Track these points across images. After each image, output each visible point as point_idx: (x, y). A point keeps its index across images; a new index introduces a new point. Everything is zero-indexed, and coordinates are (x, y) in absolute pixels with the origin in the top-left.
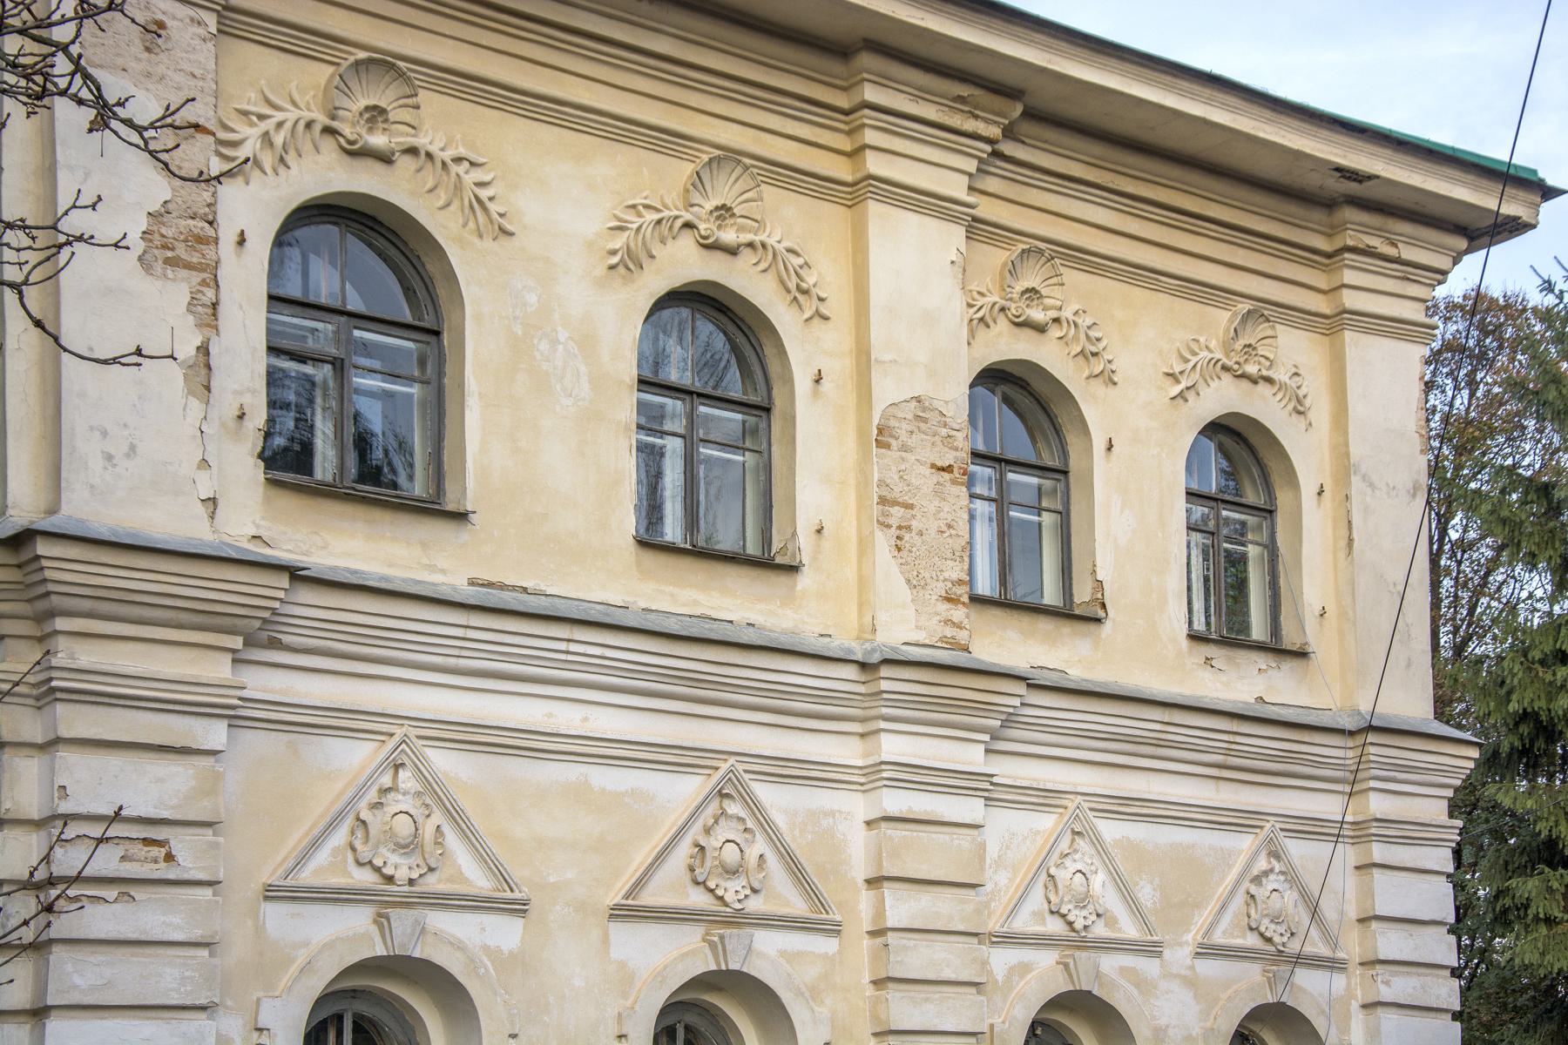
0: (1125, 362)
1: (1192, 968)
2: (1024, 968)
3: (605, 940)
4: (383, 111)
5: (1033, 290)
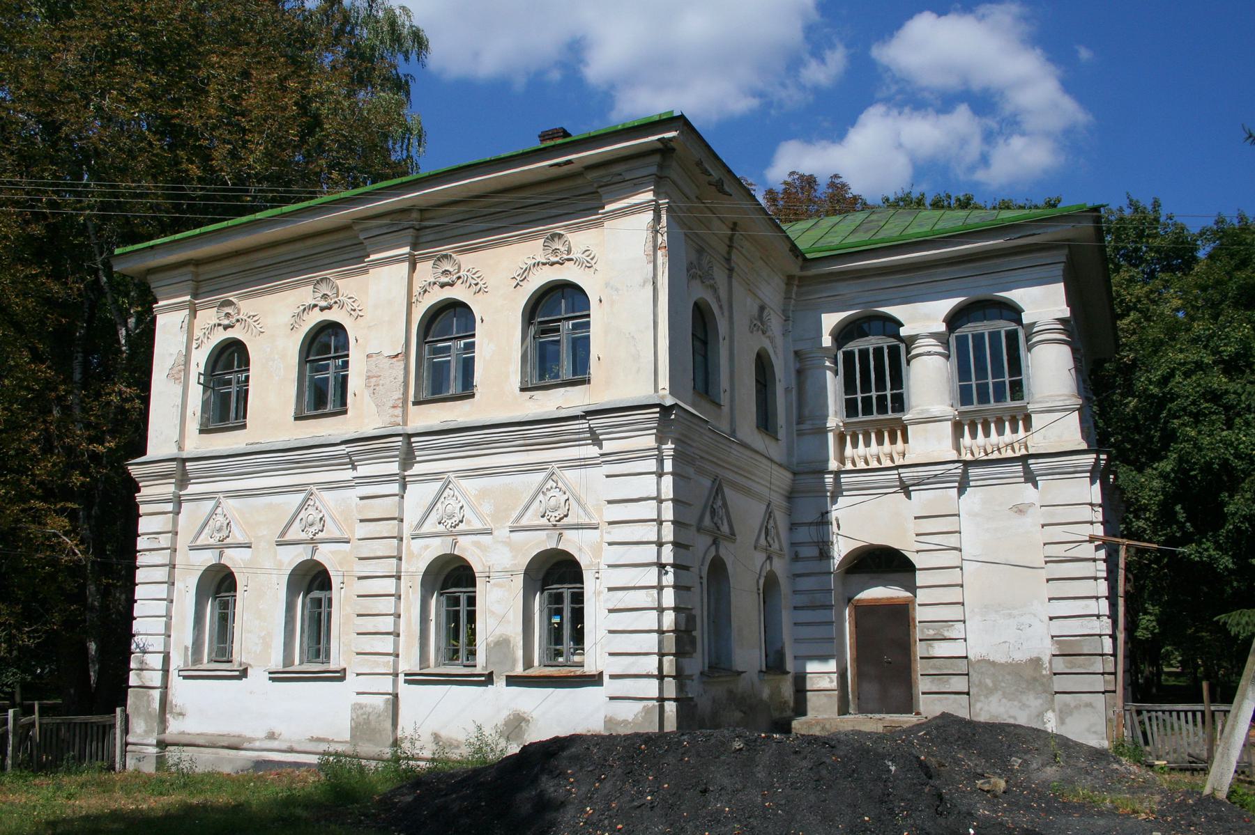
0: (491, 281)
1: (509, 537)
2: (427, 547)
3: (276, 552)
4: (229, 314)
5: (324, 294)
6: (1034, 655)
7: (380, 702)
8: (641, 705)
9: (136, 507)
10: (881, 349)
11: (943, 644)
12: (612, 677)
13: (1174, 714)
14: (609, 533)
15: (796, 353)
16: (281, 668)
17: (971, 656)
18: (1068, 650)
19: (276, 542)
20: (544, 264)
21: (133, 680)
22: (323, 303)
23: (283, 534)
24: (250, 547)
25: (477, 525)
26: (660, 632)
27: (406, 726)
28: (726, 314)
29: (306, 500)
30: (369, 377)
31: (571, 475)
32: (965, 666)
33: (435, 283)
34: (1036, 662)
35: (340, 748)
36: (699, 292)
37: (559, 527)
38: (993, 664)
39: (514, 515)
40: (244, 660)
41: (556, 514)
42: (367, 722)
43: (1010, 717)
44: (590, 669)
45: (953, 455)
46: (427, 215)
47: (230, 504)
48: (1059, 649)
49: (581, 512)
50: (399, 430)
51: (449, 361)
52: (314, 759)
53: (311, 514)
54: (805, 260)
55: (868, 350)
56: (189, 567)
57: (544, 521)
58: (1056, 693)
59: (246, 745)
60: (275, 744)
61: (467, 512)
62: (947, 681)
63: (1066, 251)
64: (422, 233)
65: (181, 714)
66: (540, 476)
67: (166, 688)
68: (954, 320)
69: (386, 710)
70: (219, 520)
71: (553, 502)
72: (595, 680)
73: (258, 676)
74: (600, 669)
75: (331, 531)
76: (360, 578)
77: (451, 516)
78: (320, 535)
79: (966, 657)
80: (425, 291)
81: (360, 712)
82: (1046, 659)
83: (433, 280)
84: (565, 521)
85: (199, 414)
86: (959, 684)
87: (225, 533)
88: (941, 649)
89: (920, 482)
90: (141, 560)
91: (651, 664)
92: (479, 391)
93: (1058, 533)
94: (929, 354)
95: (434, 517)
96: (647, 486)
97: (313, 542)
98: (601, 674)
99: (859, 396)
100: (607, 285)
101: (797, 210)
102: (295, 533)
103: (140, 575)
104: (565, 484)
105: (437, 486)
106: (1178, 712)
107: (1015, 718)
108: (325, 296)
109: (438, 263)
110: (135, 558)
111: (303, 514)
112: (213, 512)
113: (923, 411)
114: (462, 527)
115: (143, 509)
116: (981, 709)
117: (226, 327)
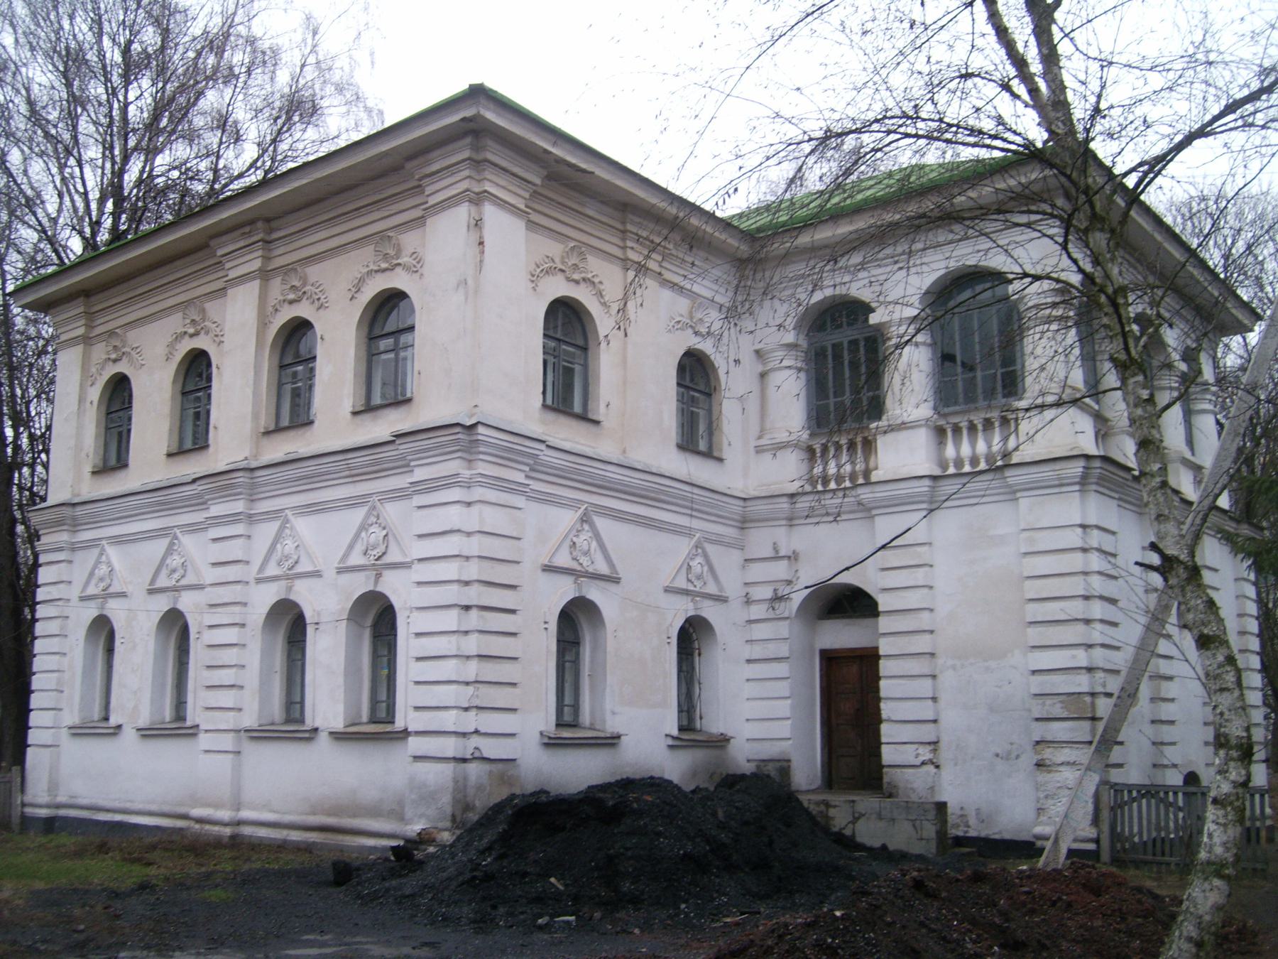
15: (757, 352)
19: (337, 568)
20: (377, 271)
22: (191, 331)
23: (153, 581)
29: (171, 544)
33: (284, 301)
36: (557, 288)
44: (399, 724)
46: (274, 224)
47: (113, 552)
53: (175, 561)
55: (841, 344)
64: (272, 246)
70: (103, 570)
72: (405, 734)
73: (129, 734)
78: (183, 582)
80: (276, 310)
83: (282, 298)
95: (359, 547)
101: (1183, 215)
102: (163, 582)
109: (287, 278)
112: (98, 563)
117: (115, 361)
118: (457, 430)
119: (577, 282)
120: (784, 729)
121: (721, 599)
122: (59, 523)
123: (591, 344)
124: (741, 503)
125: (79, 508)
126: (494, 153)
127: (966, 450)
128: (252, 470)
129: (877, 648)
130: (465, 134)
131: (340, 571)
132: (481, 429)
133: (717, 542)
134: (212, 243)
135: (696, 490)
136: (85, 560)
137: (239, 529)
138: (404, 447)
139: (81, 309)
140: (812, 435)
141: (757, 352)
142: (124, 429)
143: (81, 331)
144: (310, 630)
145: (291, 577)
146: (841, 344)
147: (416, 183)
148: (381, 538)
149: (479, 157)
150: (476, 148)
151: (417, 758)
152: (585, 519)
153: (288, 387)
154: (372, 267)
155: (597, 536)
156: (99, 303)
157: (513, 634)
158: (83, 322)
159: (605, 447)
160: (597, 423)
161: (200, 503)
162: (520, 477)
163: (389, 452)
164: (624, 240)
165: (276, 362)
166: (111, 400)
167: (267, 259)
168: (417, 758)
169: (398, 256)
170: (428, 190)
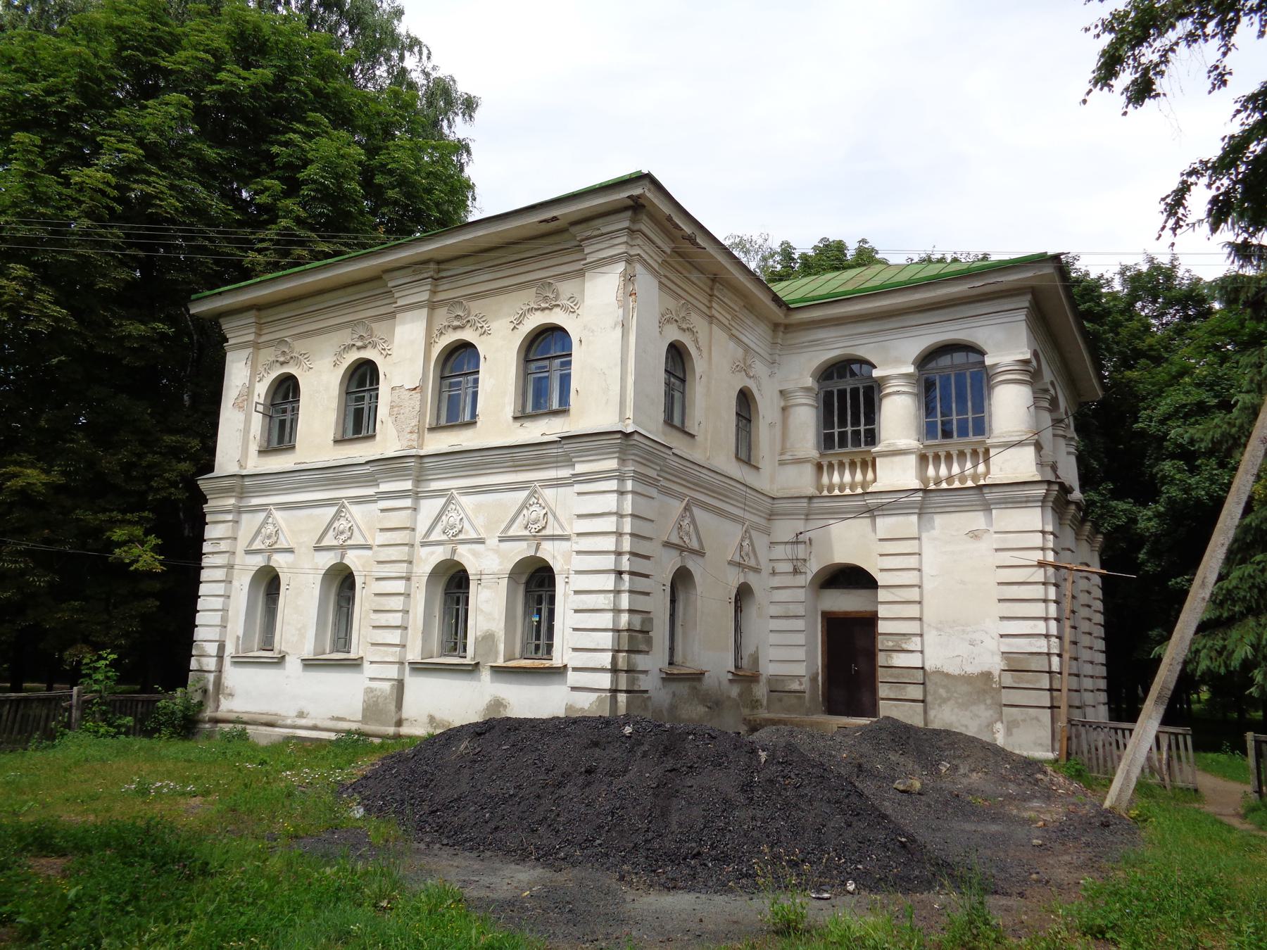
2: (433, 553)
6: (985, 669)
7: (387, 686)
8: (595, 695)
9: (204, 515)
10: (858, 389)
11: (902, 655)
12: (575, 669)
13: (1120, 732)
14: (577, 543)
15: (781, 392)
16: (312, 657)
17: (927, 667)
18: (1016, 665)
20: (536, 309)
21: (194, 664)
22: (359, 344)
24: (293, 552)
25: (473, 535)
26: (616, 630)
27: (409, 710)
28: (705, 354)
29: (339, 511)
30: (392, 407)
31: (549, 494)
32: (924, 676)
34: (987, 676)
35: (354, 726)
36: (673, 334)
37: (539, 537)
38: (947, 675)
39: (503, 527)
40: (283, 649)
41: (536, 526)
42: (376, 704)
43: (963, 726)
44: (557, 661)
45: (916, 484)
46: (442, 267)
47: (279, 515)
48: (1008, 665)
49: (556, 525)
50: (413, 452)
51: (459, 395)
52: (332, 736)
53: (342, 524)
54: (789, 309)
55: (845, 390)
56: (244, 569)
57: (526, 533)
58: (1005, 705)
59: (280, 722)
60: (303, 722)
61: (466, 524)
62: (904, 688)
63: (1029, 297)
64: (440, 282)
65: (231, 695)
66: (525, 493)
67: (220, 671)
68: (925, 360)
69: (391, 693)
70: (270, 529)
71: (534, 515)
72: (560, 671)
73: (293, 664)
74: (565, 662)
75: (357, 539)
76: (378, 579)
77: (453, 527)
78: (349, 542)
79: (922, 668)
81: (372, 695)
82: (996, 673)
83: (447, 324)
84: (543, 533)
85: (258, 437)
86: (916, 692)
87: (273, 539)
88: (900, 660)
89: (880, 507)
90: (206, 561)
91: (605, 659)
92: (481, 420)
93: (1007, 558)
94: (898, 393)
96: (610, 503)
97: (343, 548)
98: (566, 666)
99: (836, 431)
100: (585, 327)
102: (329, 541)
103: (205, 575)
104: (545, 500)
105: (442, 501)
106: (1123, 730)
107: (966, 726)
108: (361, 337)
110: (201, 560)
111: (336, 524)
112: (265, 523)
113: (889, 445)
114: (461, 536)
115: (208, 518)
116: (935, 717)
117: (282, 363)
118: (619, 436)
119: (684, 330)
120: (801, 670)
121: (757, 570)
122: (227, 491)
123: (688, 378)
124: (769, 500)
125: (246, 479)
126: (645, 226)
127: (943, 471)
128: (422, 457)
129: (876, 613)
130: (626, 209)
131: (502, 540)
132: (636, 437)
133: (757, 529)
134: (385, 277)
135: (748, 491)
136: (250, 522)
137: (408, 502)
138: (568, 447)
139: (253, 320)
140: (822, 455)
141: (781, 392)
142: (288, 417)
143: (251, 337)
144: (472, 585)
145: (455, 541)
146: (845, 390)
147: (577, 243)
148: (542, 516)
149: (636, 227)
150: (633, 221)
151: (574, 689)
152: (687, 508)
153: (446, 395)
154: (533, 305)
155: (693, 521)
156: (269, 316)
157: (648, 594)
158: (253, 330)
159: (697, 456)
160: (692, 436)
161: (372, 480)
162: (653, 474)
163: (553, 450)
164: (710, 301)
165: (439, 374)
166: (275, 393)
167: (434, 292)
168: (574, 689)
169: (556, 298)
170: (587, 250)
